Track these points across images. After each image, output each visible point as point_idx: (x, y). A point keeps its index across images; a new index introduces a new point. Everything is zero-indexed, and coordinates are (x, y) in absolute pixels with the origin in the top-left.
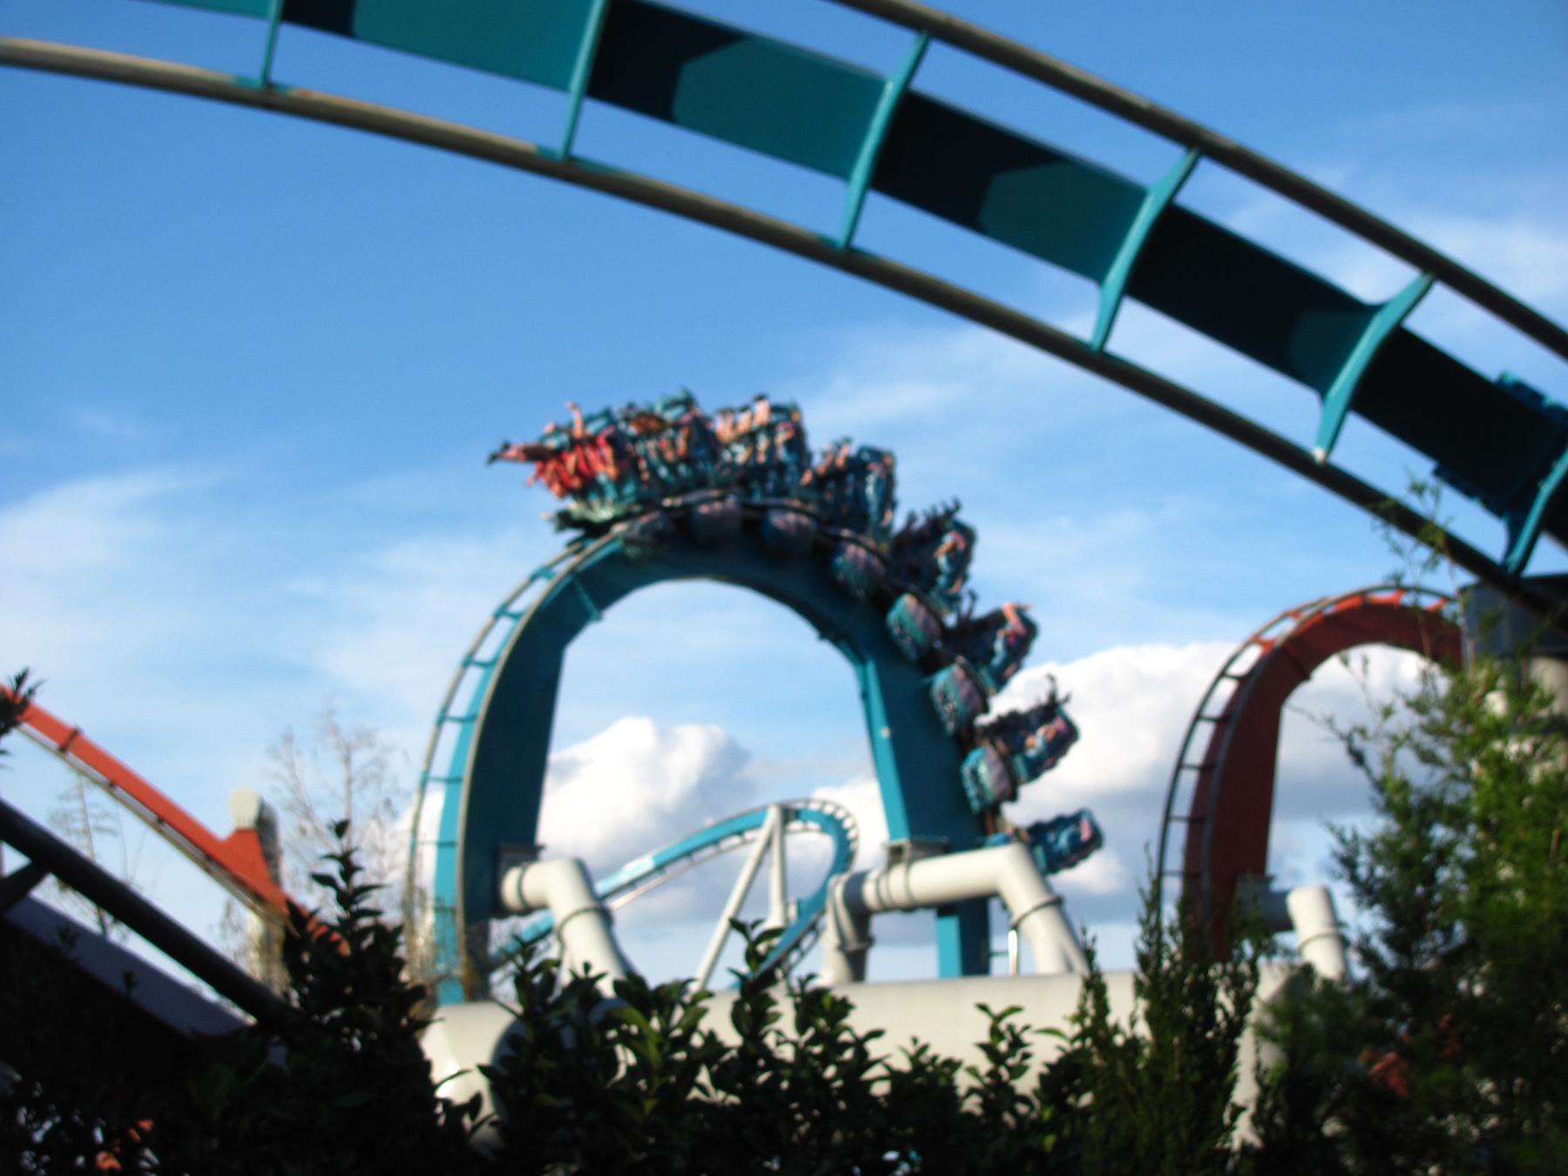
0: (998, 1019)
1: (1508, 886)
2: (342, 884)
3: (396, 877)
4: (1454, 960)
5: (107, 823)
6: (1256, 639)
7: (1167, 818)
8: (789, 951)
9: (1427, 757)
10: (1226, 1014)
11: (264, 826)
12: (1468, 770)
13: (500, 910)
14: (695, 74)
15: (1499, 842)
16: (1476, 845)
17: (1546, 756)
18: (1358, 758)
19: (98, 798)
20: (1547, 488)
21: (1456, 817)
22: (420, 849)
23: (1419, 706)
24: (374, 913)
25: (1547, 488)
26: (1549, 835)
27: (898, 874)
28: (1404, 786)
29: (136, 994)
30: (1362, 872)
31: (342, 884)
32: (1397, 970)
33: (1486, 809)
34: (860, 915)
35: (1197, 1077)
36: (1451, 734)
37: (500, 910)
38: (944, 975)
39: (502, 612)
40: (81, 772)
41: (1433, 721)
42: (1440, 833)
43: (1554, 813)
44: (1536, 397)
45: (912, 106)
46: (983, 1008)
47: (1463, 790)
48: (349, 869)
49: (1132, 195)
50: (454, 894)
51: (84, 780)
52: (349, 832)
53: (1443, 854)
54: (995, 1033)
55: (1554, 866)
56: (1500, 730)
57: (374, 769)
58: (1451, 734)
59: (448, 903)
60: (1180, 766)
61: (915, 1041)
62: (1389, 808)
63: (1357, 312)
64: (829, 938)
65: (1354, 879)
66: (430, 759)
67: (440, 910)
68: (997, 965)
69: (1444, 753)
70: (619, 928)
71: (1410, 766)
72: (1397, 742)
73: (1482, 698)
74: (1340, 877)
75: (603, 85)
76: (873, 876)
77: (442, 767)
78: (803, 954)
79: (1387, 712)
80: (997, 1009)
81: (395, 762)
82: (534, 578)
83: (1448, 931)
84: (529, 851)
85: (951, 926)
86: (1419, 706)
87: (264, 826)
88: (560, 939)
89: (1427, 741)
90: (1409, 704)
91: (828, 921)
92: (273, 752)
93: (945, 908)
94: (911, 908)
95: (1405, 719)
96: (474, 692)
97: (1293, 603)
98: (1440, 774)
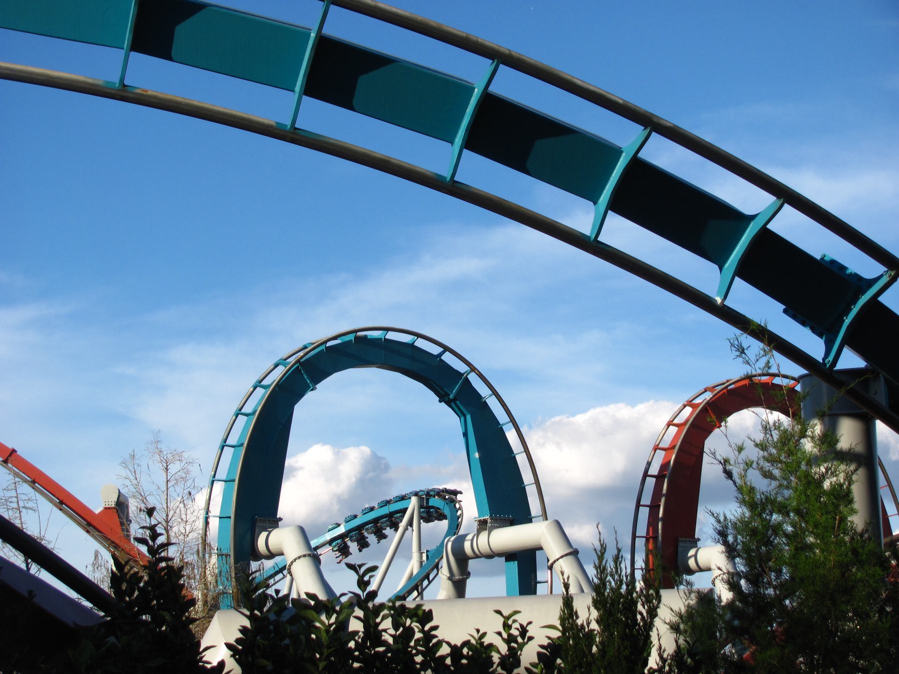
0: (507, 618)
1: (811, 547)
2: (151, 543)
3: (195, 537)
4: (786, 589)
5: (30, 505)
6: (690, 403)
7: (638, 505)
8: (422, 580)
9: (767, 475)
10: (643, 618)
11: (121, 505)
12: (790, 482)
13: (257, 556)
14: (365, 83)
15: (807, 522)
16: (794, 525)
17: (834, 474)
18: (729, 474)
19: (25, 489)
20: (847, 321)
21: (783, 509)
22: (211, 520)
23: (762, 446)
24: (167, 559)
25: (847, 321)
26: (835, 519)
27: (484, 536)
28: (752, 490)
29: (35, 600)
30: (730, 539)
31: (151, 543)
32: (750, 595)
33: (799, 504)
34: (462, 559)
35: (627, 652)
36: (781, 462)
37: (257, 556)
38: (509, 594)
39: (258, 385)
40: (16, 475)
41: (771, 454)
42: (776, 517)
43: (837, 506)
44: (843, 268)
45: (489, 101)
46: (499, 612)
47: (787, 493)
48: (155, 535)
49: (615, 152)
50: (229, 546)
51: (17, 479)
52: (155, 513)
53: (777, 529)
54: (507, 626)
55: (837, 536)
56: (813, 461)
57: (182, 474)
58: (781, 462)
59: (225, 552)
60: (646, 475)
61: (478, 631)
62: (743, 502)
63: (741, 220)
64: (444, 572)
65: (725, 543)
66: (481, 376)
67: (220, 555)
68: (541, 589)
69: (776, 472)
70: (322, 567)
71: (755, 478)
72: (748, 465)
73: (798, 441)
74: (718, 542)
75: (311, 90)
76: (469, 537)
77: (222, 473)
78: (430, 582)
79: (740, 449)
80: (506, 613)
81: (194, 470)
82: (276, 366)
83: (779, 572)
84: (273, 521)
85: (514, 565)
86: (762, 446)
87: (121, 505)
88: (290, 573)
89: (767, 466)
90: (757, 445)
91: (444, 563)
92: (124, 464)
93: (510, 556)
94: (491, 556)
95: (754, 453)
96: (242, 430)
97: (711, 384)
98: (774, 484)
